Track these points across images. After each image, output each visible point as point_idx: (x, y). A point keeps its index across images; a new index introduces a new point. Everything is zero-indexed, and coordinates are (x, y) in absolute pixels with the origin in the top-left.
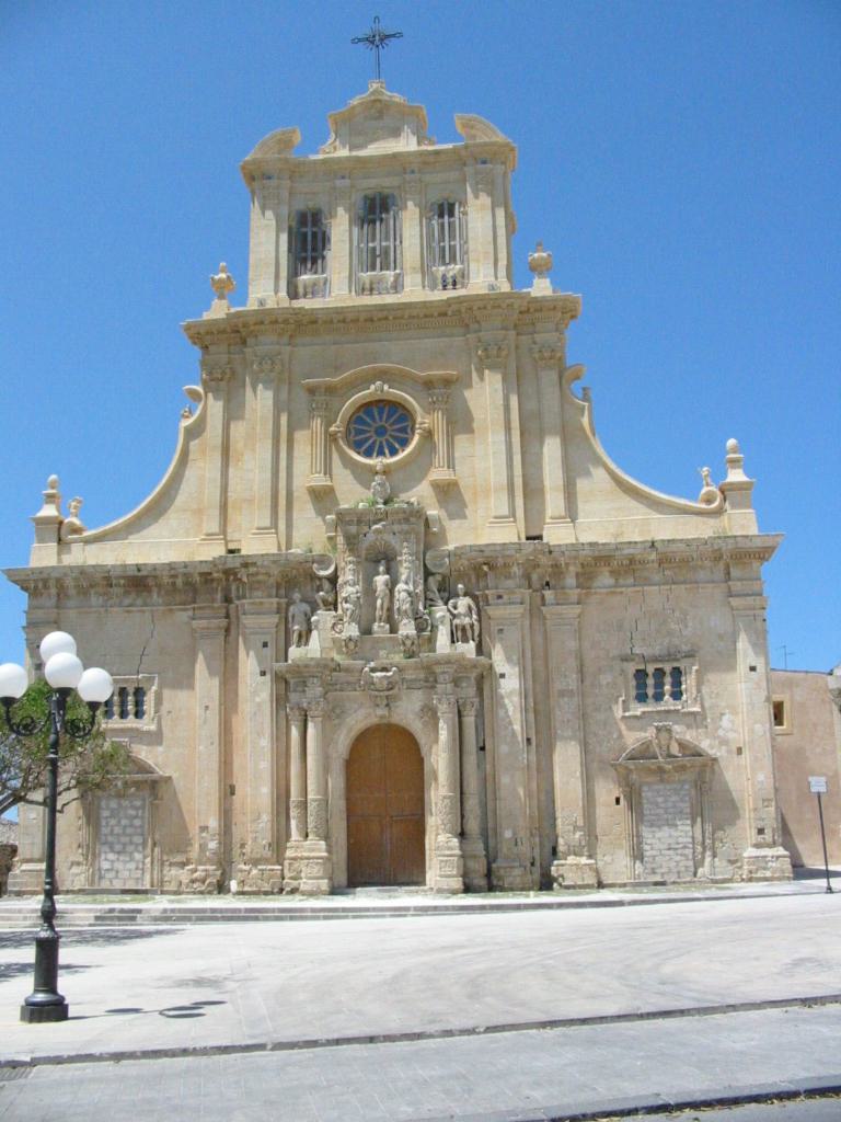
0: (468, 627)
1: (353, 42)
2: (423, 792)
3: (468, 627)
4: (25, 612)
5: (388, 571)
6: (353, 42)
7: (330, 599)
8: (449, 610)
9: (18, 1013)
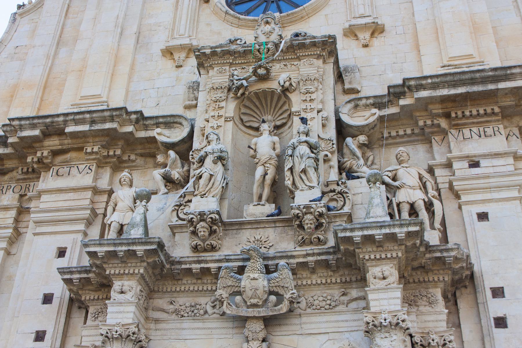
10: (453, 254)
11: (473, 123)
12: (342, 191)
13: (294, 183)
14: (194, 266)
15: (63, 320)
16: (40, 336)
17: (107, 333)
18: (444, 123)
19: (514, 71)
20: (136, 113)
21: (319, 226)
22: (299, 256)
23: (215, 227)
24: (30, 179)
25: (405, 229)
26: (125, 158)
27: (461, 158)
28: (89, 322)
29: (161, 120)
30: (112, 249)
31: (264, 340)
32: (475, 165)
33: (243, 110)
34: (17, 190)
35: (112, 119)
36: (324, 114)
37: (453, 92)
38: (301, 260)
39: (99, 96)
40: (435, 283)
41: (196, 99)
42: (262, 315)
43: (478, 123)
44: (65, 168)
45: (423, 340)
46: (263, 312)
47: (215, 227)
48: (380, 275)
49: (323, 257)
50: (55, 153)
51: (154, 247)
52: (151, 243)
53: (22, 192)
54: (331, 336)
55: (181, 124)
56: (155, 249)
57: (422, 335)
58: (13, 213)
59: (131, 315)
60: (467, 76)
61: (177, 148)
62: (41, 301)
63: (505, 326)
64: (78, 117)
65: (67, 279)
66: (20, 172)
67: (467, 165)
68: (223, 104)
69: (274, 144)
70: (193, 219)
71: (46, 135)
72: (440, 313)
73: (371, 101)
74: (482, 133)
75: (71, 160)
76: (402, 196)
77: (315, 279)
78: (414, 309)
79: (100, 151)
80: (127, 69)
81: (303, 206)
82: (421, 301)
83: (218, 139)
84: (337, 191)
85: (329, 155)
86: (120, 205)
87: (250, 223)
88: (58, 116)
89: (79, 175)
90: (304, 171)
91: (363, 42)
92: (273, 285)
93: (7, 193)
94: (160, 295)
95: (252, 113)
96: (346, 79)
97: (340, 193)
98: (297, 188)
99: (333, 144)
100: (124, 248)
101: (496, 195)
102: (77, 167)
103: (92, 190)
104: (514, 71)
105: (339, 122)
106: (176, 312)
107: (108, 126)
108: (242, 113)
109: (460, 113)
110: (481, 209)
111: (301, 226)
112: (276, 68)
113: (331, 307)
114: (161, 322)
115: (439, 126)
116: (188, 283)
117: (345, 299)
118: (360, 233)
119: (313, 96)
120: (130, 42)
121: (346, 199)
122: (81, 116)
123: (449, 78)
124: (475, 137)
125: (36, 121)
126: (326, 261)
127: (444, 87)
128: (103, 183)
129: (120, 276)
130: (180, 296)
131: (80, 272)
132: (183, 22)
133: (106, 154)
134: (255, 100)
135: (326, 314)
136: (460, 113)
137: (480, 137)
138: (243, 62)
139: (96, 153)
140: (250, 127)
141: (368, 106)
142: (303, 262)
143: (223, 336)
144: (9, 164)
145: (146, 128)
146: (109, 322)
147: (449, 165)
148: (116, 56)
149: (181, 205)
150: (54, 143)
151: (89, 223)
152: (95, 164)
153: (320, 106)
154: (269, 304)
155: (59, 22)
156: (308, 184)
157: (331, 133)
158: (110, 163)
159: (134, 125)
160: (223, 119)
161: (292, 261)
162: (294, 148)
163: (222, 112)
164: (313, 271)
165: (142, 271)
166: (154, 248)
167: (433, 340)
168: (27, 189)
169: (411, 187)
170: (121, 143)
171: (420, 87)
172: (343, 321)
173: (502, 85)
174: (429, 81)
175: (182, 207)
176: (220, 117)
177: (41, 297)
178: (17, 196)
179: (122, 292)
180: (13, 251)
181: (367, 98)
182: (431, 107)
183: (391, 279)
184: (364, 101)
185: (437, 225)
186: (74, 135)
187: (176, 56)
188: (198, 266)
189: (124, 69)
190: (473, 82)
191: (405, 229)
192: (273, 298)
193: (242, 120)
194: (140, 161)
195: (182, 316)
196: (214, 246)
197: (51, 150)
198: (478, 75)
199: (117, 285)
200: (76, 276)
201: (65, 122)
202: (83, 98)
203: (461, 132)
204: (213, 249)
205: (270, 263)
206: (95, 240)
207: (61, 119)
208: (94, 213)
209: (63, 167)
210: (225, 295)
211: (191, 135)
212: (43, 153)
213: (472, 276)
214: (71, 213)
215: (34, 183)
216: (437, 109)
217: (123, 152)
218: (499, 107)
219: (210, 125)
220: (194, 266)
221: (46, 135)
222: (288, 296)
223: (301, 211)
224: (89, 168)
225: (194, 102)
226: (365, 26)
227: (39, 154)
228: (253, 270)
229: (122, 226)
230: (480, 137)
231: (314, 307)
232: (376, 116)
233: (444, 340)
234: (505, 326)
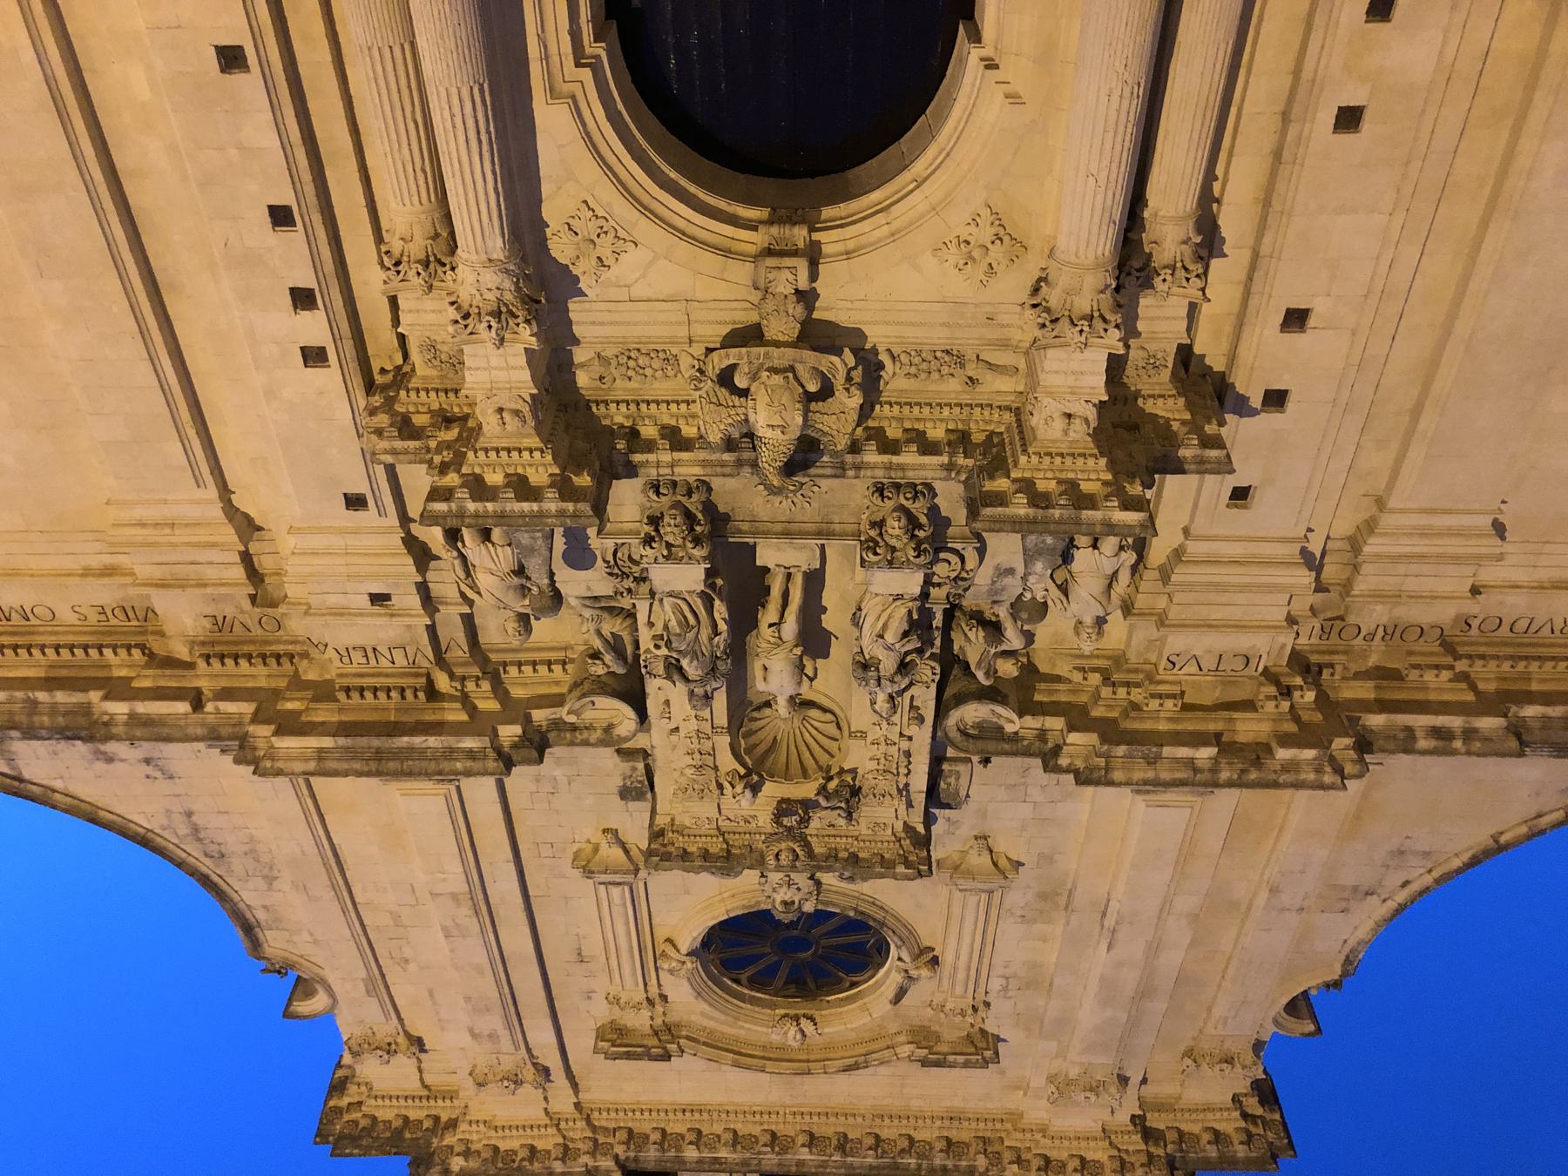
11: (387, 675)
12: (619, 580)
13: (710, 609)
16: (1296, 319)
17: (1106, 330)
21: (655, 521)
23: (873, 533)
24: (1323, 652)
29: (1007, 747)
32: (378, 599)
38: (685, 455)
42: (762, 350)
43: (379, 675)
44: (1228, 670)
45: (442, 275)
47: (873, 533)
55: (964, 733)
56: (987, 506)
57: (443, 284)
59: (1048, 365)
61: (974, 687)
63: (294, 292)
65: (1212, 447)
66: (1339, 668)
67: (394, 600)
69: (765, 679)
70: (916, 554)
73: (579, 737)
74: (371, 655)
79: (1145, 698)
81: (683, 561)
82: (452, 353)
84: (631, 579)
87: (804, 534)
89: (1198, 653)
92: (740, 411)
93: (1375, 626)
94: (999, 398)
95: (819, 737)
97: (625, 575)
98: (703, 595)
99: (646, 667)
102: (1201, 669)
103: (1167, 622)
108: (837, 740)
112: (765, 820)
113: (627, 353)
114: (997, 342)
115: (452, 676)
121: (612, 563)
124: (383, 649)
130: (953, 396)
133: (1134, 691)
135: (637, 340)
137: (374, 649)
138: (832, 839)
139: (1153, 696)
140: (825, 710)
141: (586, 728)
142: (680, 450)
143: (858, 304)
150: (1249, 728)
152: (1161, 671)
154: (747, 370)
156: (680, 602)
158: (1129, 671)
159: (1065, 744)
162: (713, 670)
165: (1023, 459)
166: (988, 509)
167: (419, 274)
168: (1327, 630)
172: (602, 324)
175: (953, 575)
177: (1290, 405)
186: (1198, 740)
193: (839, 728)
195: (947, 352)
196: (876, 495)
197: (1256, 711)
201: (1214, 770)
203: (411, 662)
209: (1234, 674)
211: (941, 711)
212: (1277, 706)
215: (1311, 642)
218: (338, 701)
223: (687, 552)
224: (1174, 664)
230: (374, 649)
231: (661, 355)
232: (566, 708)
233: (398, 272)
234: (294, 292)
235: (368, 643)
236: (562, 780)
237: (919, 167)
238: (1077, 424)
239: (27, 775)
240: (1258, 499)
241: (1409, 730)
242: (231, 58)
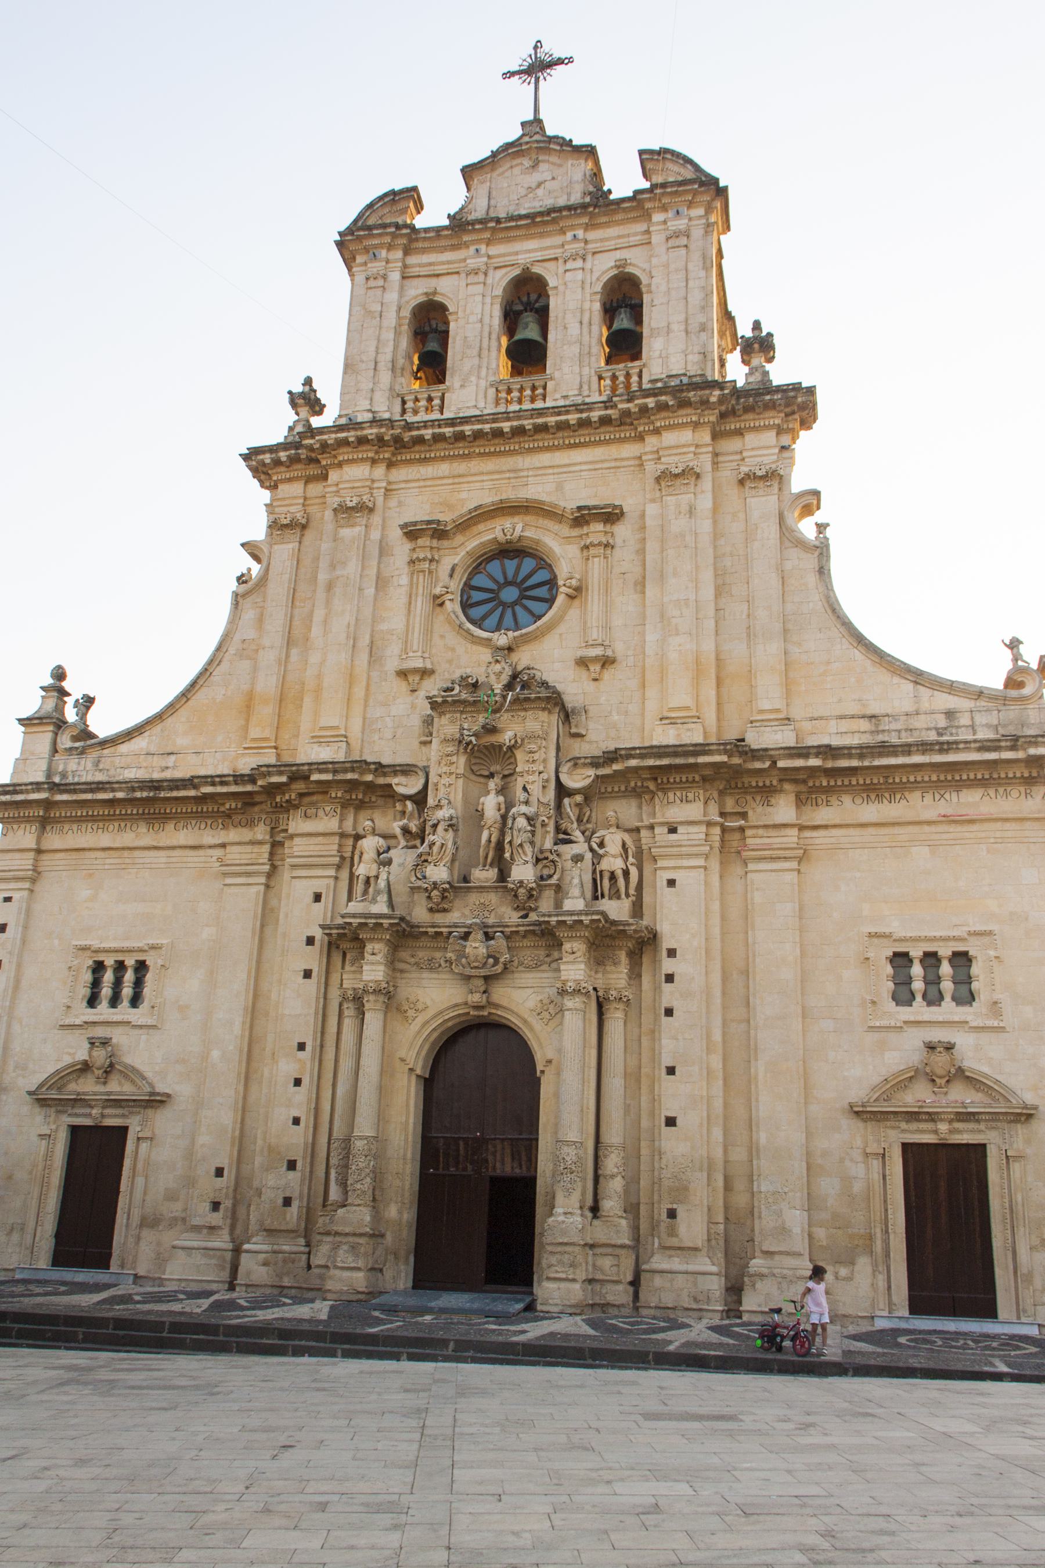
0: (619, 874)
1: (570, 60)
2: (55, 1251)
3: (619, 874)
4: (266, 505)
5: (502, 791)
6: (570, 60)
7: (414, 829)
8: (591, 850)
9: (809, 432)
10: (633, 928)
14: (429, 930)
15: (325, 960)
18: (652, 786)
19: (712, 748)
20: (375, 763)
22: (512, 926)
25: (589, 918)
26: (367, 800)
27: (662, 824)
28: (347, 968)
30: (363, 921)
31: (484, 992)
32: (673, 830)
33: (473, 761)
34: (268, 822)
35: (353, 770)
36: (545, 776)
37: (658, 763)
38: (514, 929)
39: (337, 728)
40: (620, 948)
41: (431, 734)
46: (483, 972)
48: (570, 950)
49: (531, 928)
50: (301, 795)
51: (396, 921)
52: (395, 918)
53: (273, 825)
54: (536, 989)
58: (267, 848)
59: (382, 973)
60: (671, 750)
62: (305, 943)
64: (321, 767)
67: (666, 830)
68: (454, 759)
71: (293, 778)
72: (621, 972)
73: (589, 761)
75: (317, 802)
76: (605, 865)
77: (526, 942)
78: (601, 969)
80: (362, 693)
83: (450, 803)
85: (546, 820)
86: (365, 857)
88: (303, 765)
90: (521, 845)
91: (594, 675)
96: (573, 722)
97: (553, 861)
100: (373, 921)
101: (686, 863)
104: (712, 748)
105: (560, 786)
106: (417, 964)
107: (349, 776)
109: (665, 780)
110: (671, 875)
111: (516, 896)
115: (647, 787)
116: (424, 942)
117: (548, 960)
118: (555, 919)
119: (536, 756)
120: (363, 657)
122: (324, 766)
123: (655, 750)
124: (678, 801)
125: (282, 769)
126: (534, 931)
127: (650, 758)
128: (348, 826)
129: (372, 940)
131: (337, 928)
132: (416, 635)
134: (484, 751)
136: (665, 780)
140: (481, 775)
144: (258, 799)
145: (385, 775)
146: (365, 978)
147: (652, 827)
148: (351, 675)
149: (418, 865)
150: (300, 786)
151: (339, 867)
153: (541, 768)
155: (286, 615)
157: (551, 794)
160: (454, 776)
161: (507, 929)
163: (453, 769)
164: (524, 937)
169: (614, 856)
170: (362, 788)
171: (629, 757)
173: (701, 760)
174: (638, 752)
176: (451, 774)
177: (305, 939)
178: (268, 829)
179: (373, 954)
180: (272, 884)
181: (586, 758)
182: (640, 772)
183: (578, 954)
184: (582, 761)
185: (632, 891)
187: (411, 678)
188: (433, 930)
189: (359, 692)
190: (676, 754)
191: (589, 918)
192: (491, 961)
194: (380, 801)
198: (680, 749)
199: (369, 947)
200: (334, 931)
202: (322, 728)
204: (445, 910)
205: (490, 930)
206: (295, 498)
207: (306, 767)
208: (343, 858)
210: (454, 958)
213: (655, 935)
214: (322, 859)
216: (646, 775)
217: (365, 794)
219: (443, 781)
220: (429, 930)
221: (293, 778)
222: (502, 960)
225: (429, 739)
226: (596, 659)
227: (287, 797)
228: (475, 940)
229: (368, 878)
235: (685, 806)
236: (614, 713)
237: (427, 1047)
238: (370, 951)
239: (911, 686)
240: (310, 898)
241: (236, 784)
242: (671, 1071)
